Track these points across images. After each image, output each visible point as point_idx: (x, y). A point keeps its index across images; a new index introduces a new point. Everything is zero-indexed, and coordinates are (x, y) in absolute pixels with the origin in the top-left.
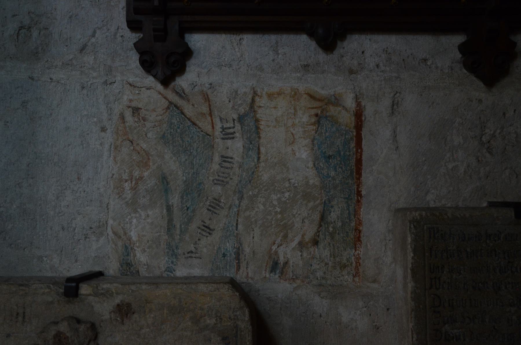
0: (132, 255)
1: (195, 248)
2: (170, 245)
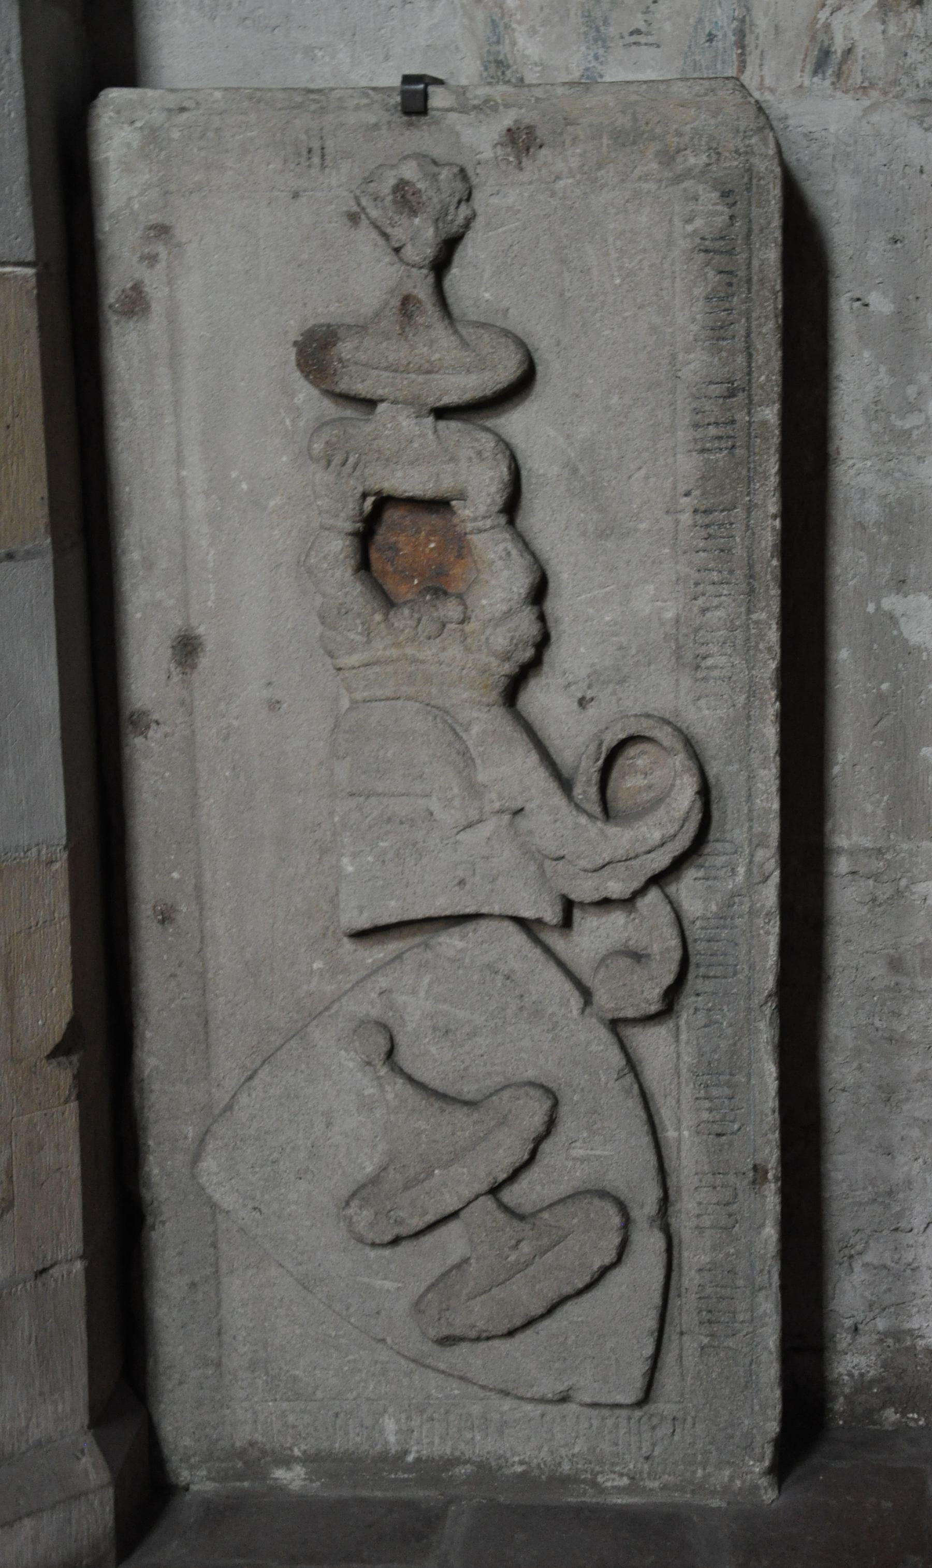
0: (507, 42)
1: (646, 21)
2: (589, 16)
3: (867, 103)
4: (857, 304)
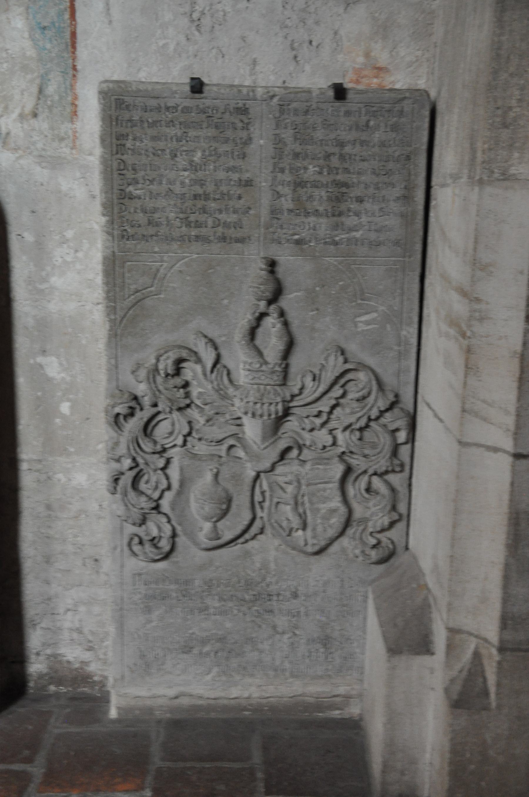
3: (17, 155)
4: (19, 237)
